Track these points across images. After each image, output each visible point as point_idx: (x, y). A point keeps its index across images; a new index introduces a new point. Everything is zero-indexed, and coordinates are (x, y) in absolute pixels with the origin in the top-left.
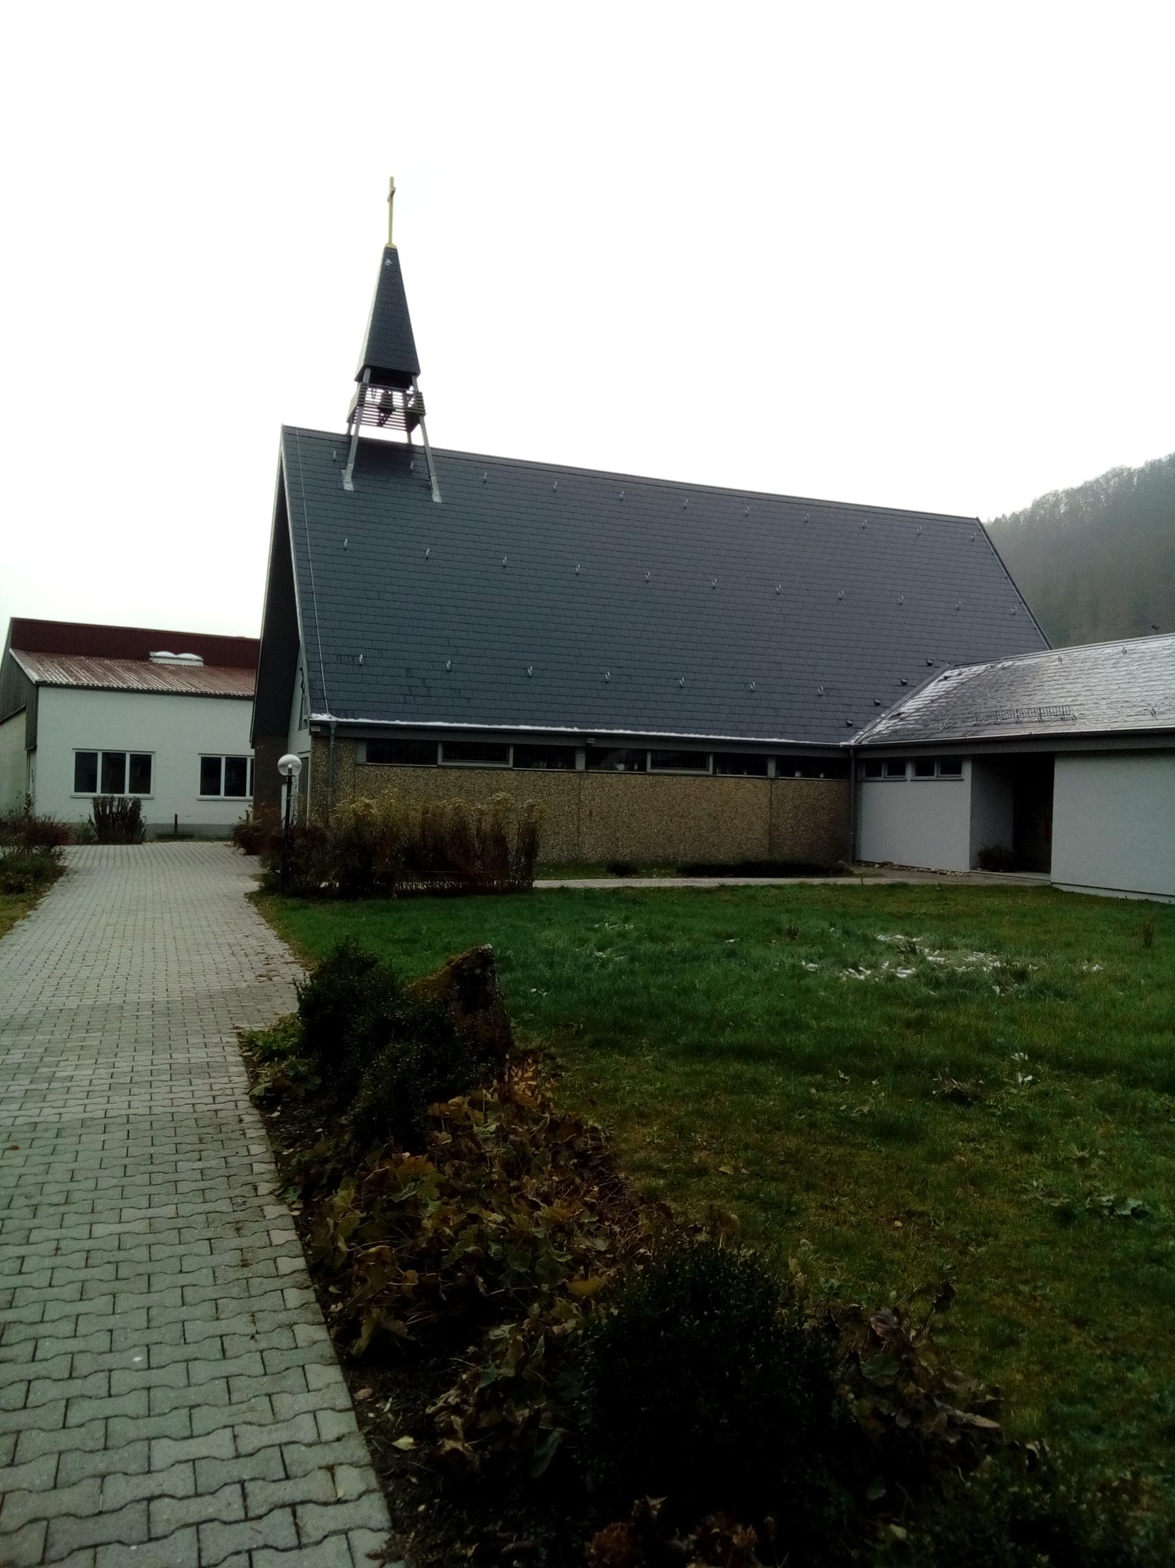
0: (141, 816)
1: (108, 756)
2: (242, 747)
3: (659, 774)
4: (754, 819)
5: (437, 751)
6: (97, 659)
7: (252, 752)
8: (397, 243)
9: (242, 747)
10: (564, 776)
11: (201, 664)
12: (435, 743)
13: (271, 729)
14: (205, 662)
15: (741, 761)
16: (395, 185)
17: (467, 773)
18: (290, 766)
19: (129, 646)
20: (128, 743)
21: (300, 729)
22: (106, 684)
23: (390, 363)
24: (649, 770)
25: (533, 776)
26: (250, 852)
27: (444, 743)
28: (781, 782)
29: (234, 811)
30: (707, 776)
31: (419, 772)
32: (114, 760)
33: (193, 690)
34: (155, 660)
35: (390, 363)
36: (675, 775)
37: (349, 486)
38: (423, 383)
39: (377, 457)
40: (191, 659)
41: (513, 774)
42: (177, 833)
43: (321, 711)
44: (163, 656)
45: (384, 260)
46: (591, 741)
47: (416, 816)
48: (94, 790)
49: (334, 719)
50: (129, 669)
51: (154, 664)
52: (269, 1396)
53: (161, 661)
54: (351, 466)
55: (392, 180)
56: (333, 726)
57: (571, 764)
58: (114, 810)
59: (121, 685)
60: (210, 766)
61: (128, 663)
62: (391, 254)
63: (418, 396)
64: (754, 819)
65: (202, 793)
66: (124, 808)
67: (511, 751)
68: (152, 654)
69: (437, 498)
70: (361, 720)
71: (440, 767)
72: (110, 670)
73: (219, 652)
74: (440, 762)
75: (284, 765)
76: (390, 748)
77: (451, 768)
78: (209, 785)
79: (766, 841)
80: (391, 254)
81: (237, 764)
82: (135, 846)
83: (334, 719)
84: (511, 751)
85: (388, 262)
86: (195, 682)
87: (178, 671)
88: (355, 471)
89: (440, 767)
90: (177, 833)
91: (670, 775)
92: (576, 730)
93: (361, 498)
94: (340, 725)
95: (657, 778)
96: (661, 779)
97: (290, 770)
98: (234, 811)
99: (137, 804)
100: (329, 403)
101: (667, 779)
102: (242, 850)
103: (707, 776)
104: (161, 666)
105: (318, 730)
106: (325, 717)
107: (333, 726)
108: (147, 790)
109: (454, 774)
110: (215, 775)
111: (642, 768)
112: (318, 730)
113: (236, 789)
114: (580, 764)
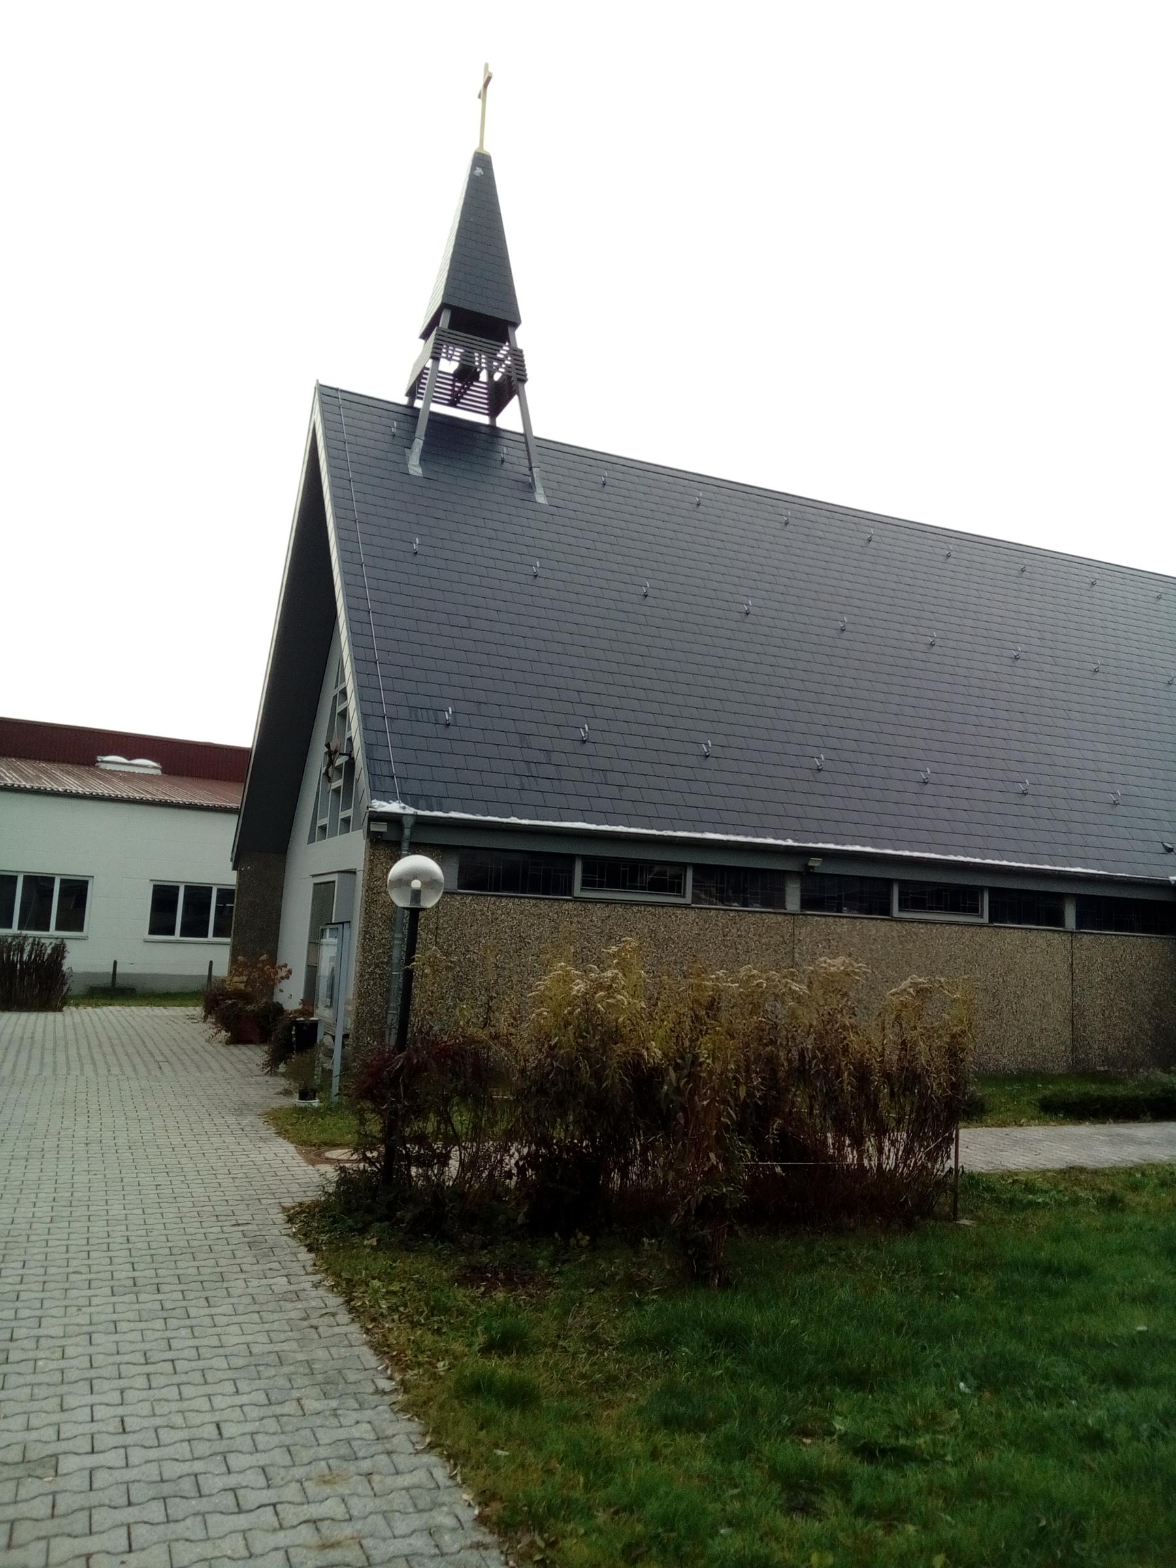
0: (64, 968)
1: (30, 880)
2: (219, 871)
3: (912, 921)
4: (1049, 998)
5: (571, 872)
6: (31, 762)
7: (230, 878)
8: (488, 149)
9: (219, 871)
10: (770, 919)
11: (159, 772)
12: (570, 859)
13: (264, 842)
14: (163, 771)
15: (1026, 901)
16: (490, 70)
17: (620, 909)
18: (416, 884)
19: (75, 747)
20: (58, 863)
21: (311, 840)
22: (36, 785)
23: (476, 314)
24: (896, 912)
25: (723, 919)
26: (238, 1038)
27: (584, 858)
28: (1086, 939)
29: (208, 957)
30: (981, 926)
31: (544, 907)
32: (39, 885)
33: (149, 797)
34: (102, 766)
35: (476, 314)
36: (934, 923)
37: (415, 468)
38: (522, 337)
39: (453, 443)
40: (147, 765)
41: (692, 915)
42: (114, 990)
43: (388, 796)
44: (113, 761)
45: (473, 168)
46: (815, 863)
47: (809, 1017)
48: (10, 926)
49: (410, 810)
50: (68, 773)
51: (102, 770)
52: (164, 1499)
53: (109, 767)
54: (419, 444)
55: (487, 66)
56: (408, 823)
57: (775, 901)
58: (25, 957)
59: (55, 787)
60: (163, 897)
61: (70, 767)
62: (482, 162)
63: (517, 356)
64: (1049, 998)
65: (152, 932)
66: (40, 954)
67: (690, 875)
68: (99, 758)
69: (541, 499)
70: (453, 814)
71: (577, 900)
72: (45, 772)
73: (185, 760)
74: (577, 891)
75: (403, 882)
76: (506, 866)
77: (596, 901)
78: (161, 922)
79: (1067, 1034)
80: (482, 162)
81: (198, 895)
82: (50, 1016)
83: (410, 810)
84: (690, 875)
85: (479, 171)
86: (150, 789)
87: (129, 777)
88: (423, 451)
89: (577, 900)
90: (114, 990)
91: (926, 922)
92: (790, 842)
93: (430, 492)
94: (421, 822)
95: (908, 926)
96: (915, 928)
97: (416, 895)
98: (208, 957)
99: (59, 951)
100: (388, 361)
101: (922, 929)
102: (224, 1035)
103: (981, 926)
104: (111, 772)
105: (382, 828)
106: (394, 807)
107: (408, 823)
108: (80, 928)
109: (599, 912)
110: (176, 909)
111: (886, 910)
112: (382, 828)
113: (196, 928)
114: (793, 901)
